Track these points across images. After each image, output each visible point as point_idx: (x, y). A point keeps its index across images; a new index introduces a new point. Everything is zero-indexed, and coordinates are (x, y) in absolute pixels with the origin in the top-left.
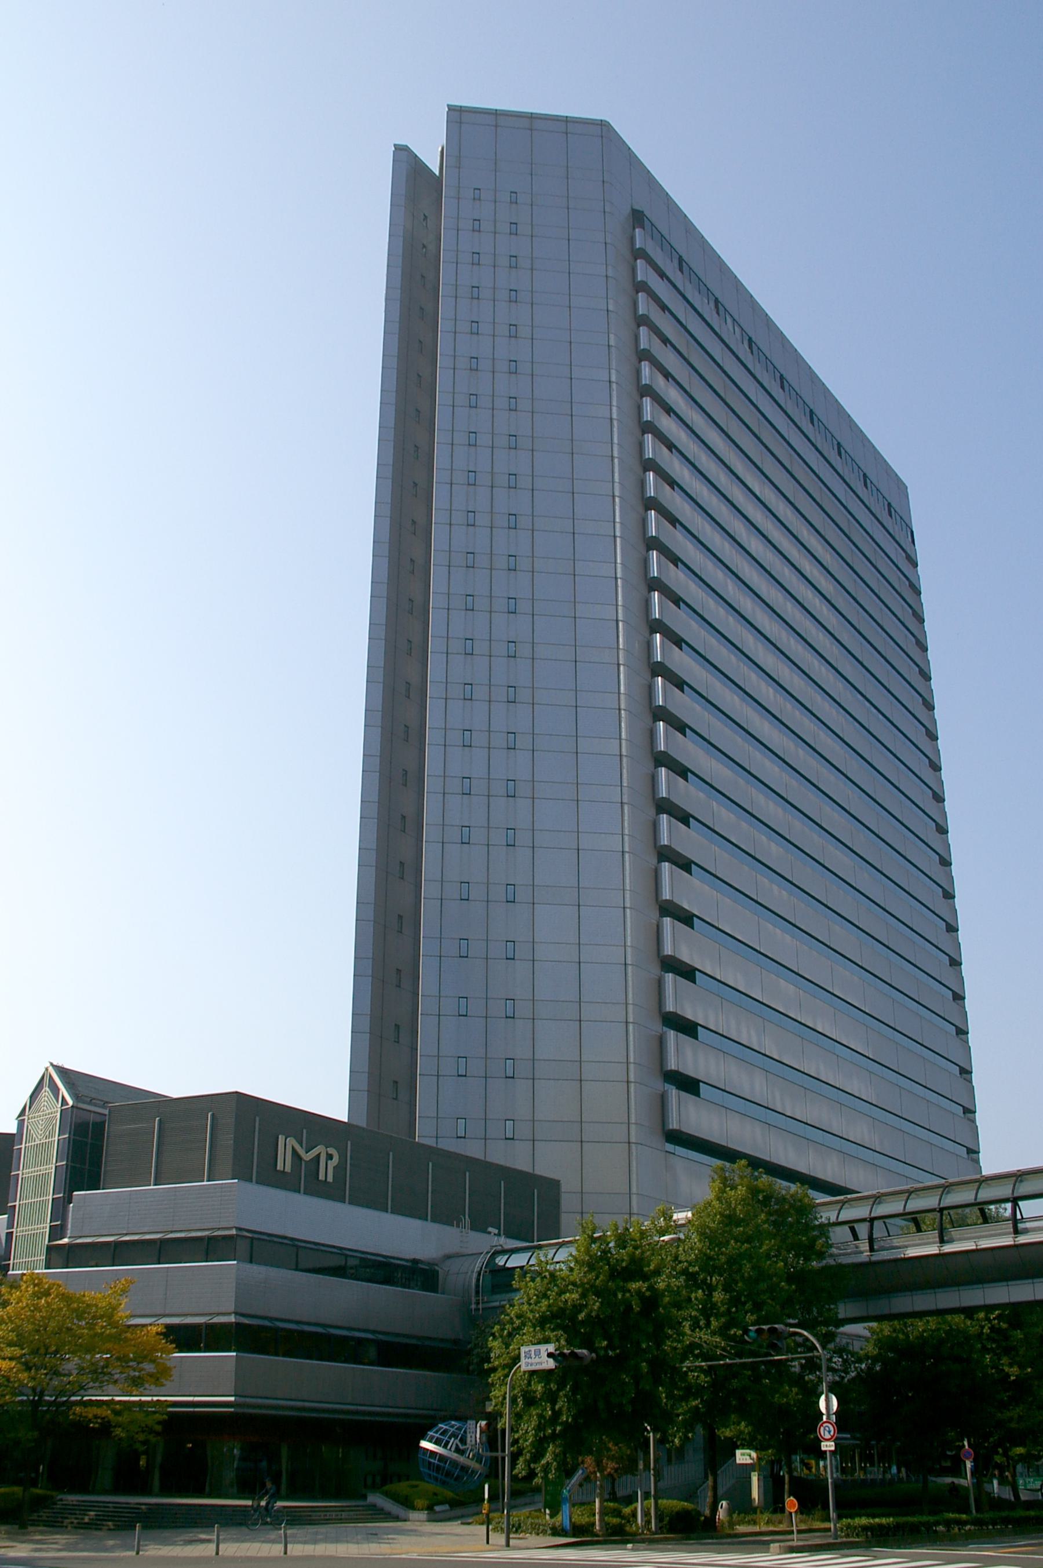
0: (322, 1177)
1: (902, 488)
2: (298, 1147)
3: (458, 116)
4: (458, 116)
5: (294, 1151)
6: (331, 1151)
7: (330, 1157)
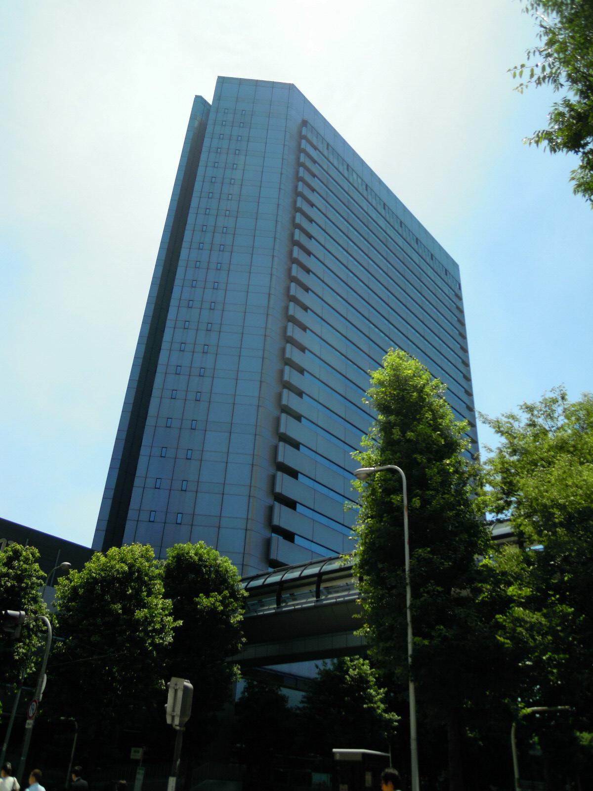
1: (456, 266)
3: (222, 82)
4: (222, 82)
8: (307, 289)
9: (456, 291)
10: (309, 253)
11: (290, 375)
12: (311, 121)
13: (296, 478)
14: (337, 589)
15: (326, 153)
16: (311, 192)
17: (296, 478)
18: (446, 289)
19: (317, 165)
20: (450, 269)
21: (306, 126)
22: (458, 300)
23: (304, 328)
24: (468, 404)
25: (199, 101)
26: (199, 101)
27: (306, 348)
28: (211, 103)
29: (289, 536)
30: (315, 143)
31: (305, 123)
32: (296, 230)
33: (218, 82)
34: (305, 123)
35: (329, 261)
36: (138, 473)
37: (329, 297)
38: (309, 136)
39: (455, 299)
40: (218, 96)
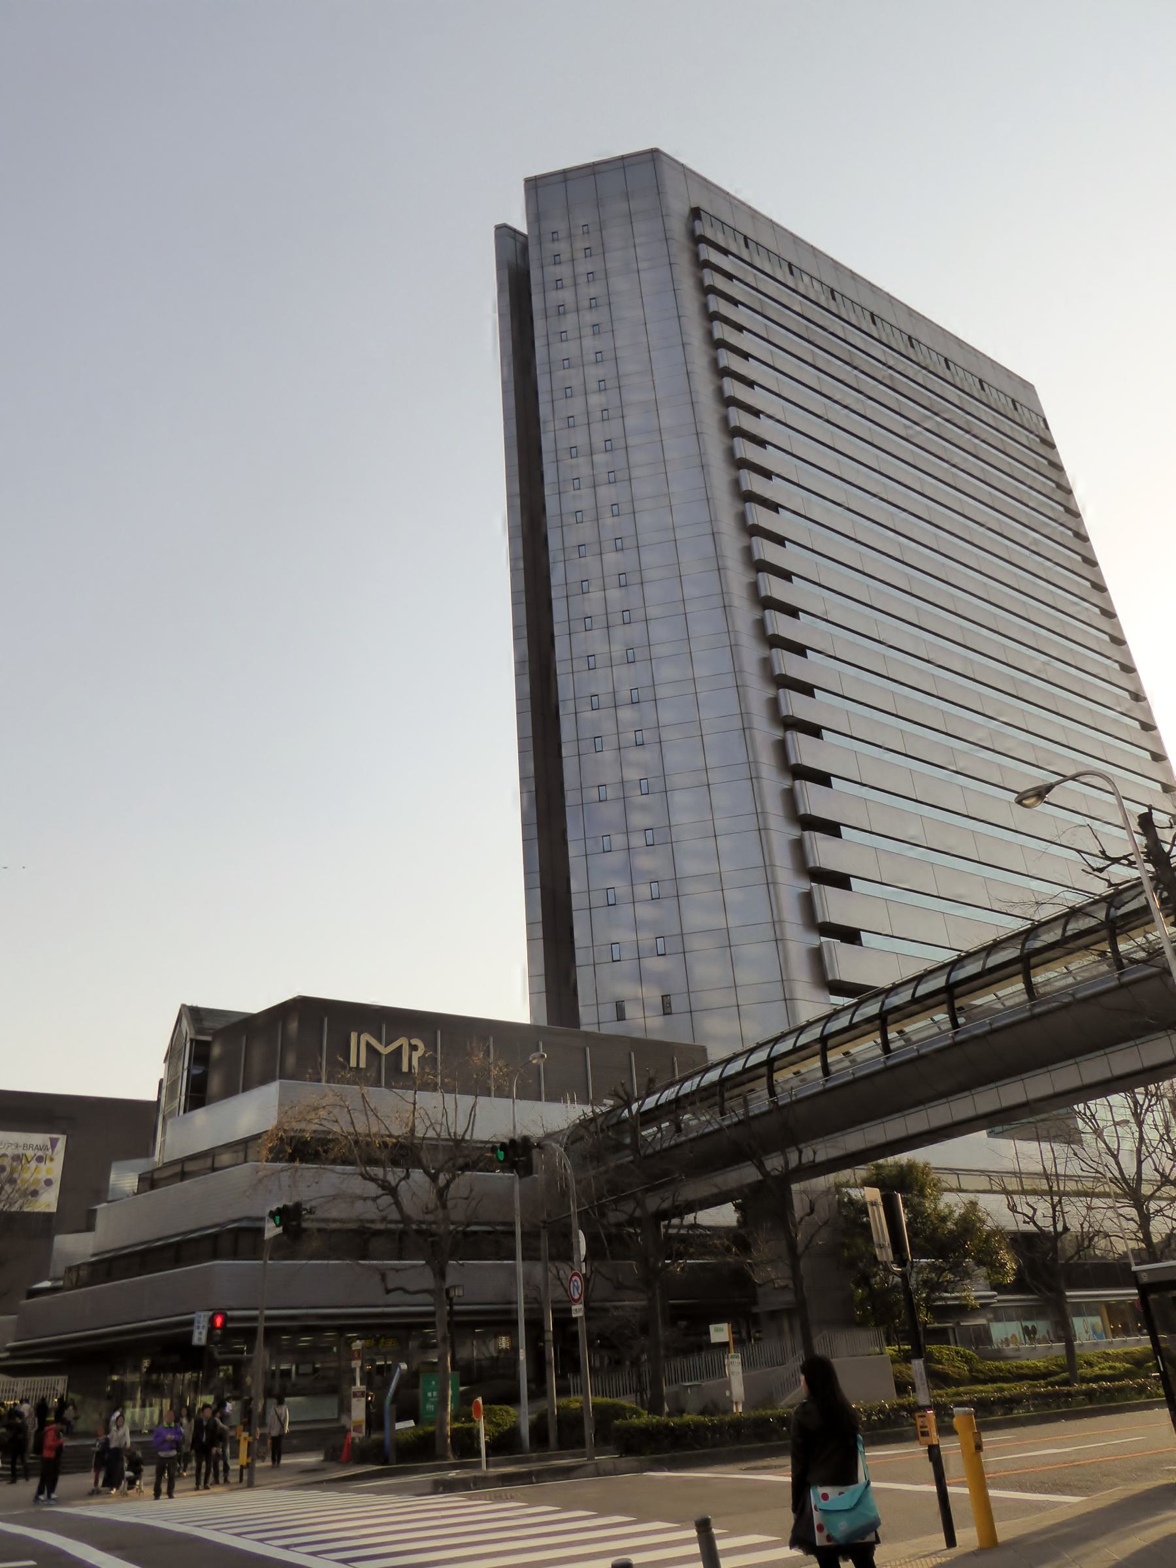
0: (405, 1068)
1: (1028, 387)
2: (374, 1042)
3: (534, 186)
4: (534, 186)
5: (369, 1046)
6: (414, 1042)
7: (414, 1048)
8: (762, 443)
9: (1042, 435)
10: (756, 413)
11: (760, 516)
12: (705, 205)
13: (828, 784)
14: (1031, 1300)
15: (745, 255)
16: (736, 332)
17: (828, 784)
18: (1022, 435)
19: (769, 447)
20: (1020, 398)
21: (700, 218)
22: (1055, 471)
23: (775, 507)
24: (1132, 689)
25: (504, 232)
26: (504, 232)
27: (762, 413)
28: (524, 230)
29: (851, 936)
30: (722, 243)
31: (696, 213)
32: (736, 439)
33: (527, 190)
34: (696, 213)
35: (818, 509)
36: (578, 943)
37: (818, 509)
38: (709, 234)
39: (1042, 449)
40: (535, 214)
